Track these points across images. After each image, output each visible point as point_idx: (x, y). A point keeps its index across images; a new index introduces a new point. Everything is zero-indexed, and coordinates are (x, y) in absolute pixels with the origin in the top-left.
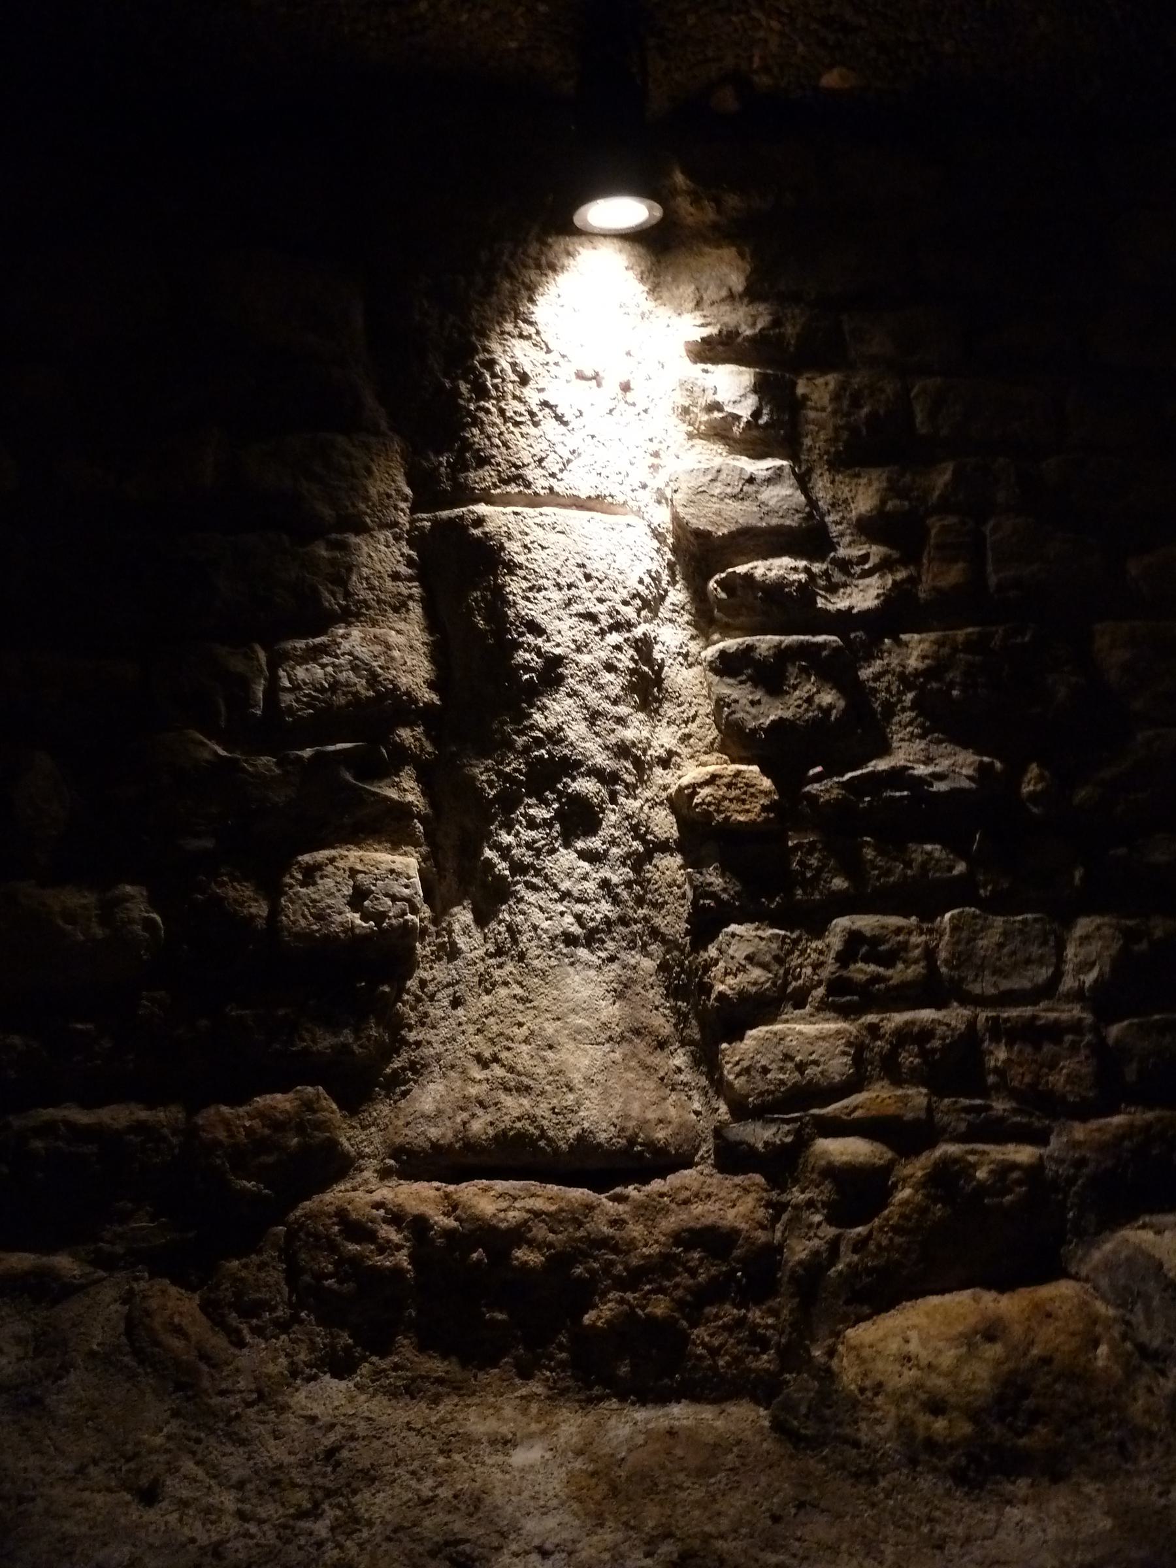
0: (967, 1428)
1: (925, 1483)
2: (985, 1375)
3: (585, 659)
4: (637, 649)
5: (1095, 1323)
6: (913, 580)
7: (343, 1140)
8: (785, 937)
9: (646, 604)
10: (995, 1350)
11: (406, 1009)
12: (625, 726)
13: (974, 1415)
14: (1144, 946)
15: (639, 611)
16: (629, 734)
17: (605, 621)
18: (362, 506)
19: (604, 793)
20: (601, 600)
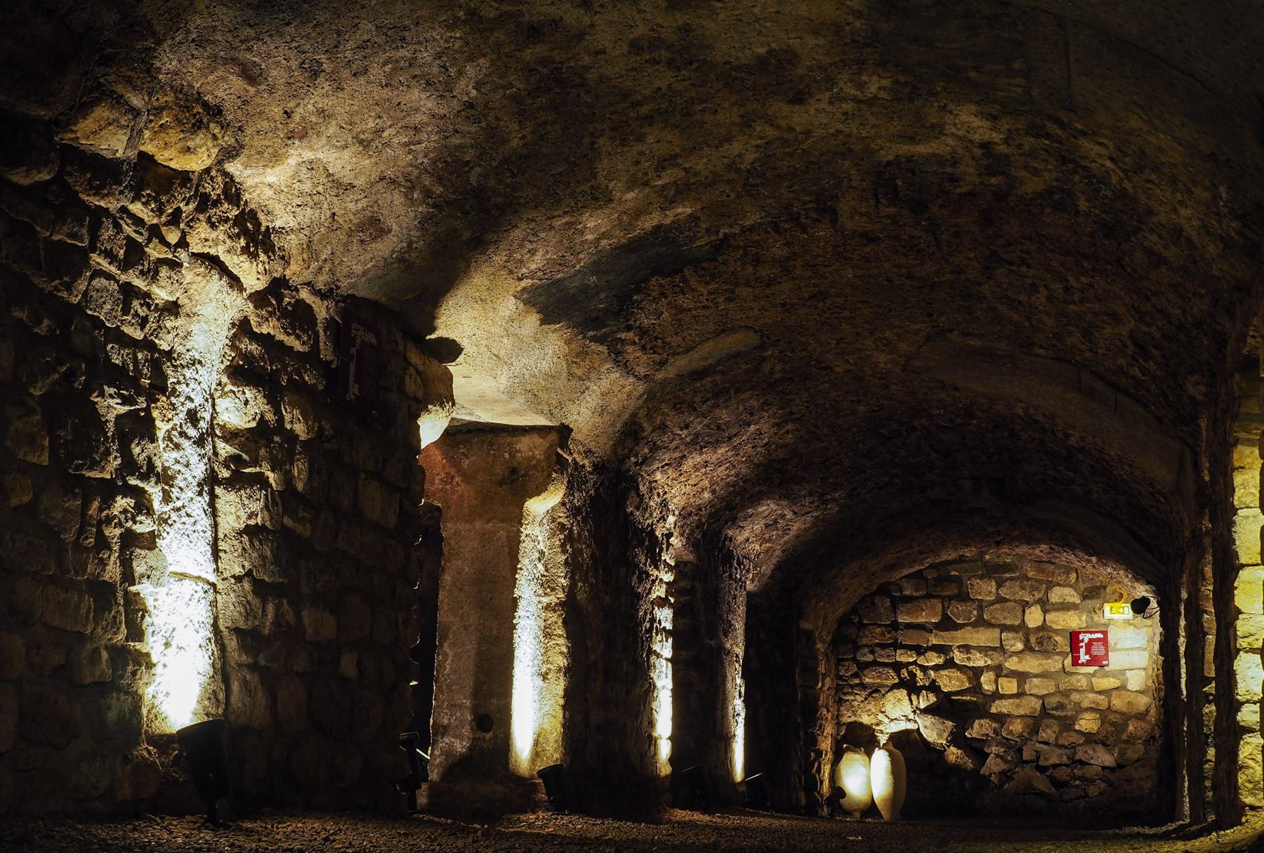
0: (212, 125)
1: (230, 117)
2: (199, 138)
3: (190, 494)
4: (170, 497)
5: (155, 132)
6: (101, 510)
7: (252, 308)
8: (156, 338)
9: (165, 521)
10: (191, 144)
11: (229, 353)
12: (176, 459)
13: (208, 128)
14: (65, 279)
15: (169, 517)
16: (175, 455)
17: (183, 512)
18: (235, 587)
19: (185, 428)
20: (184, 523)
